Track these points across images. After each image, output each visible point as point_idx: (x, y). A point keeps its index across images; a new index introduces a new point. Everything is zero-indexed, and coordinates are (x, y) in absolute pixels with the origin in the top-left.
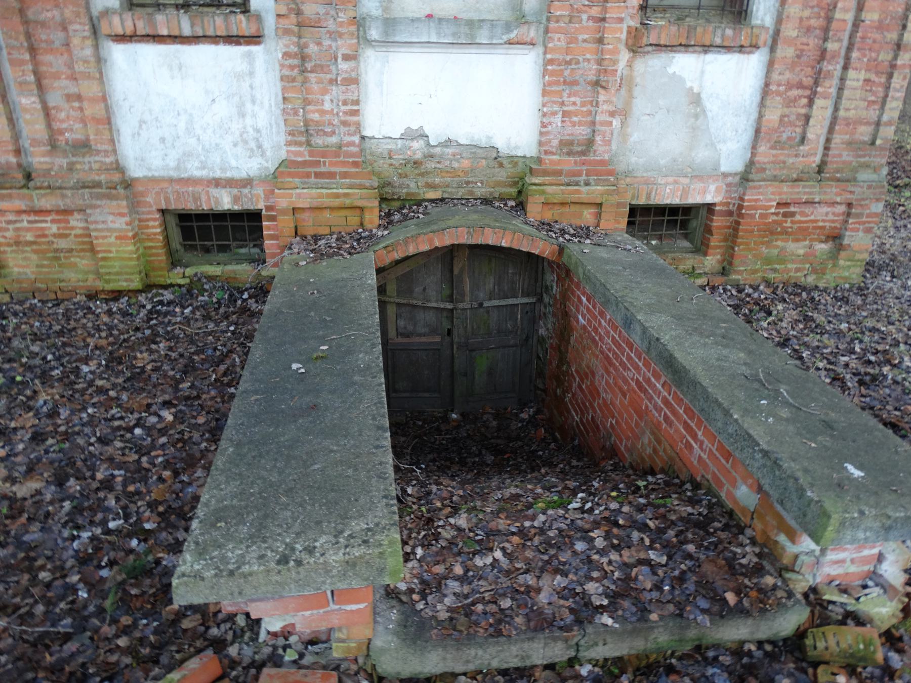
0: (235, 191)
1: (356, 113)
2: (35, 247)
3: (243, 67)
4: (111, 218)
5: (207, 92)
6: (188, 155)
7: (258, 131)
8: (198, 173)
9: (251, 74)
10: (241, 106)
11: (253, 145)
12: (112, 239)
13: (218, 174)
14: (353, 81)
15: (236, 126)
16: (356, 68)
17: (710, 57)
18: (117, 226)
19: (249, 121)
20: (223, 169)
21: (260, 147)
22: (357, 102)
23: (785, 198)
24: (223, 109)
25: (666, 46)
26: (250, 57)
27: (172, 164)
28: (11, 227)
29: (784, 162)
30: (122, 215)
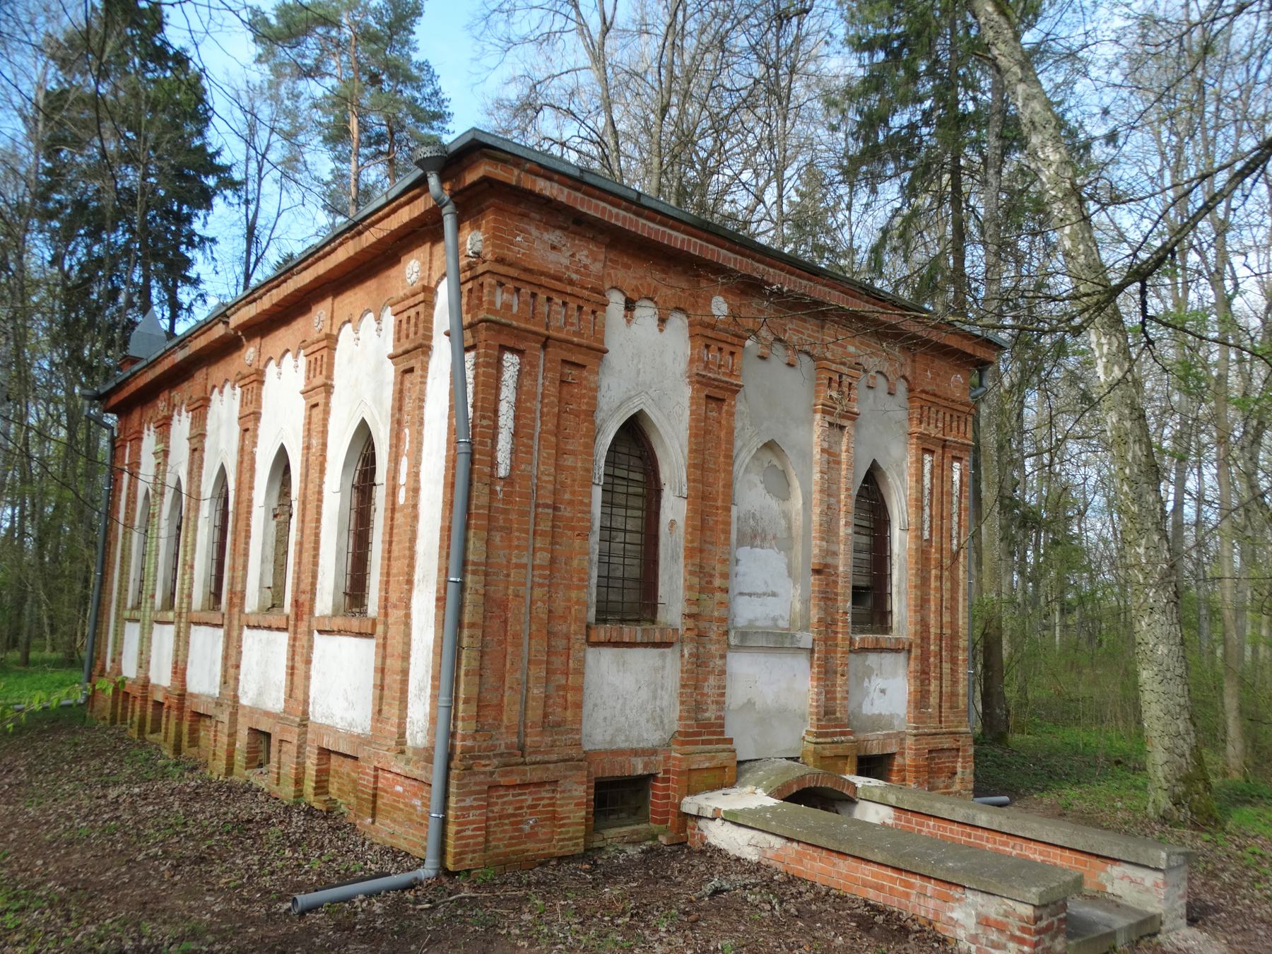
0: (646, 759)
1: (723, 695)
2: (512, 819)
3: (659, 663)
4: (575, 787)
5: (637, 681)
6: (618, 730)
7: (662, 710)
8: (623, 745)
9: (663, 668)
10: (655, 691)
11: (658, 721)
12: (572, 807)
13: (635, 746)
14: (723, 672)
15: (650, 707)
16: (725, 664)
17: (883, 655)
18: (577, 793)
19: (658, 703)
20: (638, 742)
21: (662, 722)
22: (724, 687)
23: (931, 747)
24: (645, 694)
25: (392, 519)
26: (663, 656)
27: (608, 738)
28: (500, 801)
29: (156, 729)
30: (582, 783)
